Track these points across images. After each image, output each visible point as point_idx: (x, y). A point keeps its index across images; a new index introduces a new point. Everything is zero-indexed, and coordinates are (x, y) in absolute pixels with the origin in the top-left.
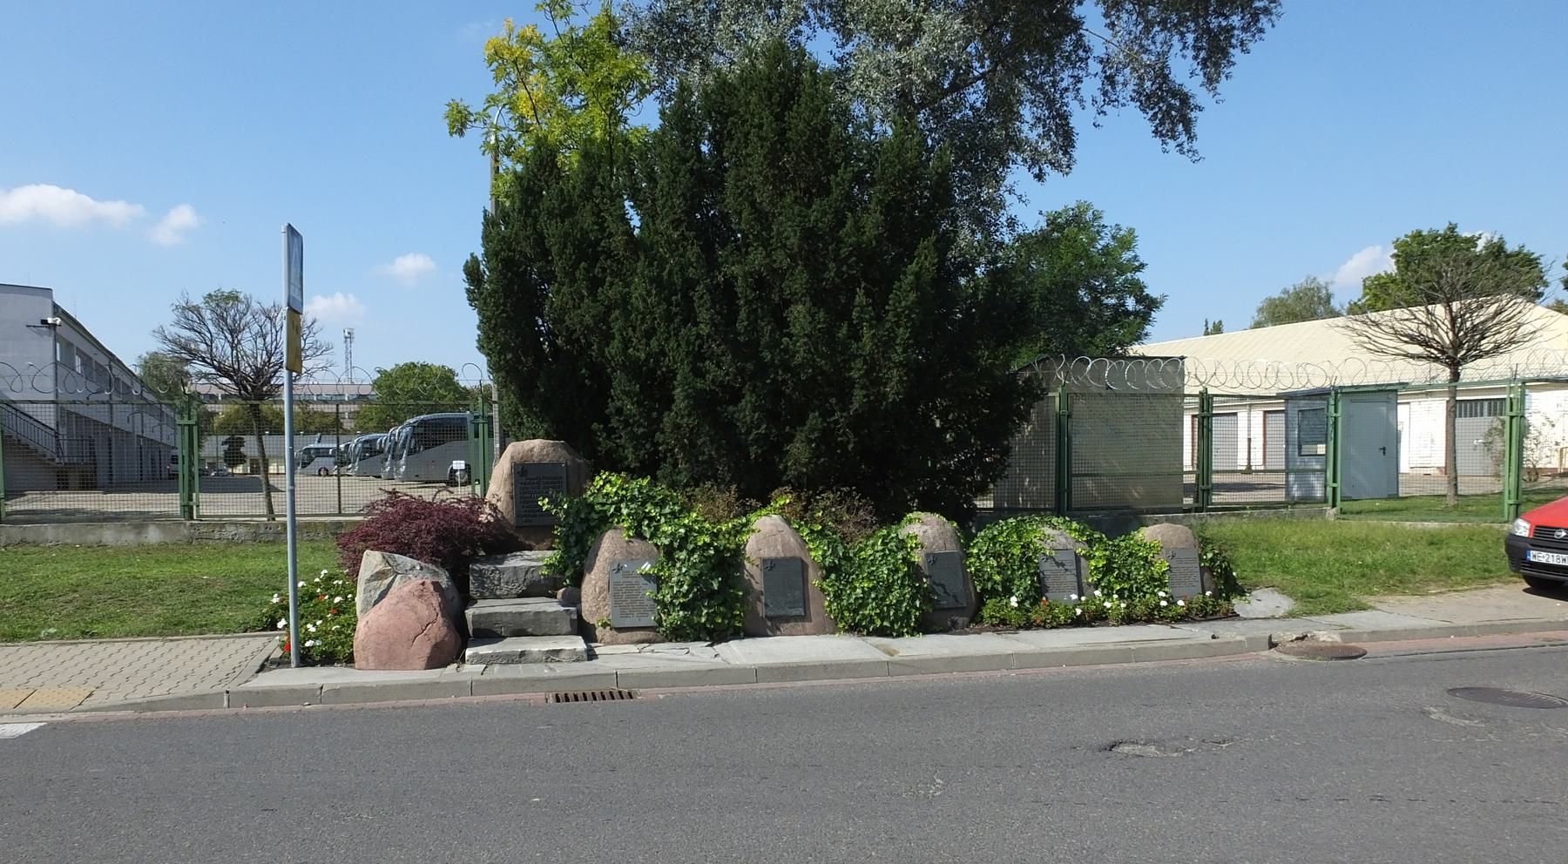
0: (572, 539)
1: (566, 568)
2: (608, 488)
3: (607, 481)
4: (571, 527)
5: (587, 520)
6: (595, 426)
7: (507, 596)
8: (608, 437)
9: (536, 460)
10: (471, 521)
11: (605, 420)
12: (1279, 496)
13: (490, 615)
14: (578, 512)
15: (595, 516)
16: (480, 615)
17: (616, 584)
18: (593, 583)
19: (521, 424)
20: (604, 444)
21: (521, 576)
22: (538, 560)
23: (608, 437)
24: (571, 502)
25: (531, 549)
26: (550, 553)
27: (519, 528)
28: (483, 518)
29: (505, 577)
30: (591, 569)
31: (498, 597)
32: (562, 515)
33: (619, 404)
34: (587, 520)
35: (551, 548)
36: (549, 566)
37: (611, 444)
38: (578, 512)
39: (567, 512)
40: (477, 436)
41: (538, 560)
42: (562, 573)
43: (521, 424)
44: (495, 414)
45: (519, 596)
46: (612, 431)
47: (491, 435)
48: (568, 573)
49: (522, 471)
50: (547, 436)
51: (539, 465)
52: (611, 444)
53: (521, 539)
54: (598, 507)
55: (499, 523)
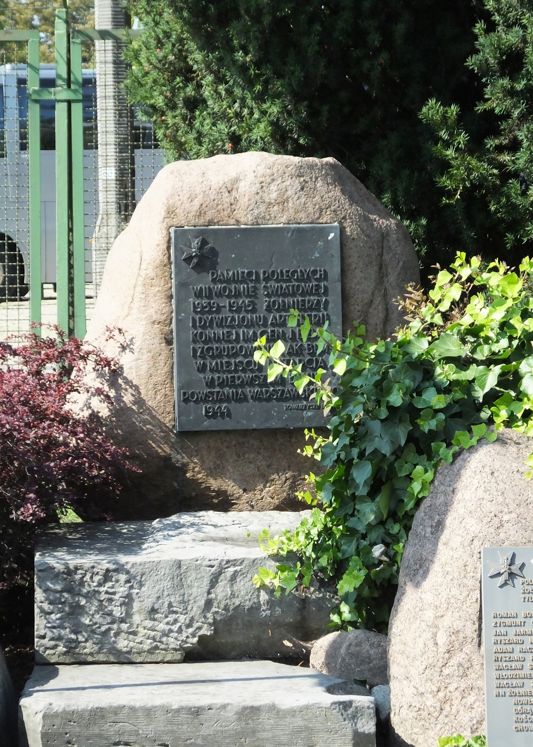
0: (362, 474)
1: (340, 567)
2: (477, 311)
3: (473, 289)
4: (359, 435)
5: (411, 412)
6: (432, 110)
7: (152, 656)
8: (475, 147)
9: (245, 218)
10: (39, 414)
11: (466, 90)
12: (78, 109)
13: (98, 714)
14: (382, 387)
15: (436, 400)
16: (69, 716)
17: (504, 620)
18: (421, 619)
19: (195, 104)
20: (461, 168)
21: (198, 592)
22: (251, 540)
23: (475, 147)
24: (357, 353)
25: (224, 504)
26: (289, 519)
27: (187, 435)
28: (77, 406)
29: (145, 596)
30: (421, 569)
31: (124, 659)
32: (327, 397)
33: (512, 38)
34: (411, 412)
35: (292, 504)
36: (288, 560)
37: (481, 168)
38: (382, 387)
39: (345, 390)
40: (48, 142)
41: (251, 540)
42: (329, 583)
43: (195, 104)
44: (102, 67)
45: (191, 656)
46: (491, 124)
47: (90, 141)
48: (347, 585)
49: (202, 255)
50: (281, 141)
51: (254, 235)
52: (481, 168)
53: (196, 471)
54: (445, 373)
55: (125, 423)
